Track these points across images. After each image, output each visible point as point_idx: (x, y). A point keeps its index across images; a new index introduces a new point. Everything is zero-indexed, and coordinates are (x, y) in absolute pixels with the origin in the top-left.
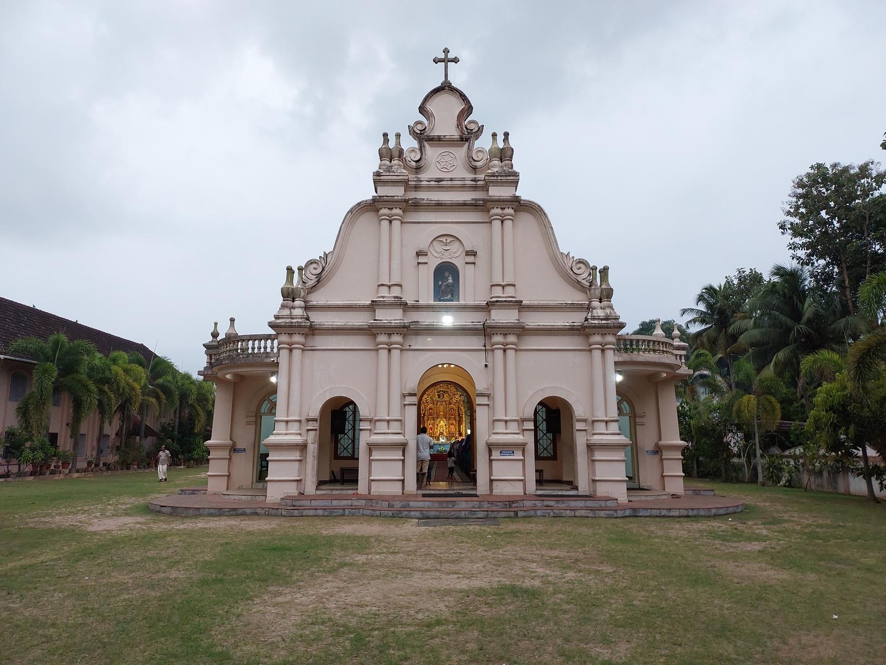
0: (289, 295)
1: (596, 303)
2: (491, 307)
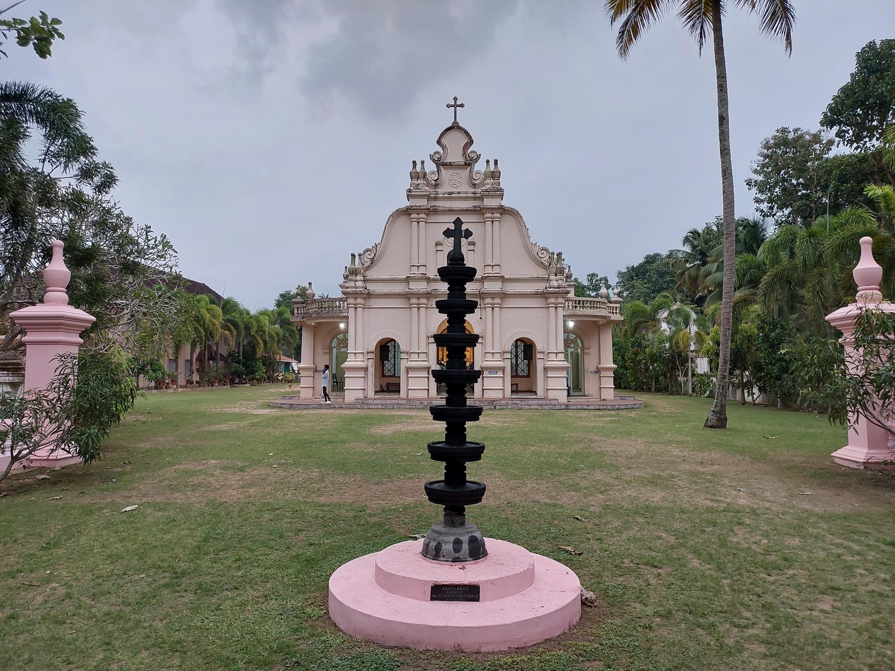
1: (553, 277)
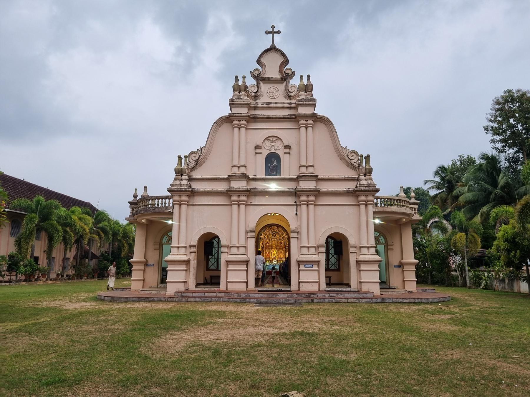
0: (179, 172)
1: (362, 177)
2: (299, 179)
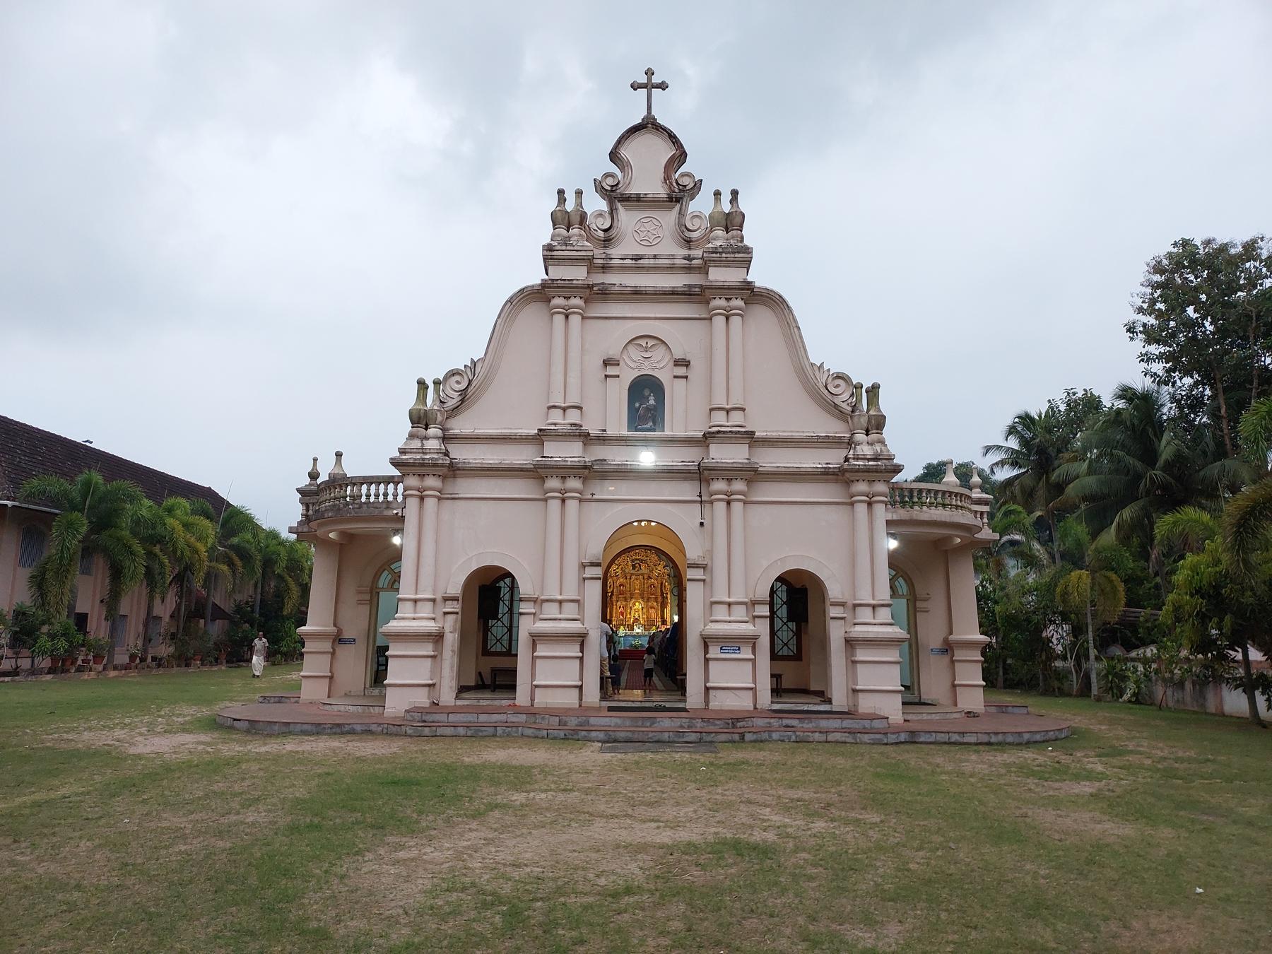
0: (420, 419)
1: (861, 437)
